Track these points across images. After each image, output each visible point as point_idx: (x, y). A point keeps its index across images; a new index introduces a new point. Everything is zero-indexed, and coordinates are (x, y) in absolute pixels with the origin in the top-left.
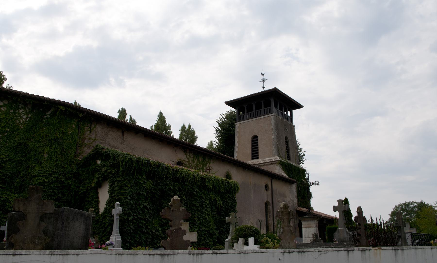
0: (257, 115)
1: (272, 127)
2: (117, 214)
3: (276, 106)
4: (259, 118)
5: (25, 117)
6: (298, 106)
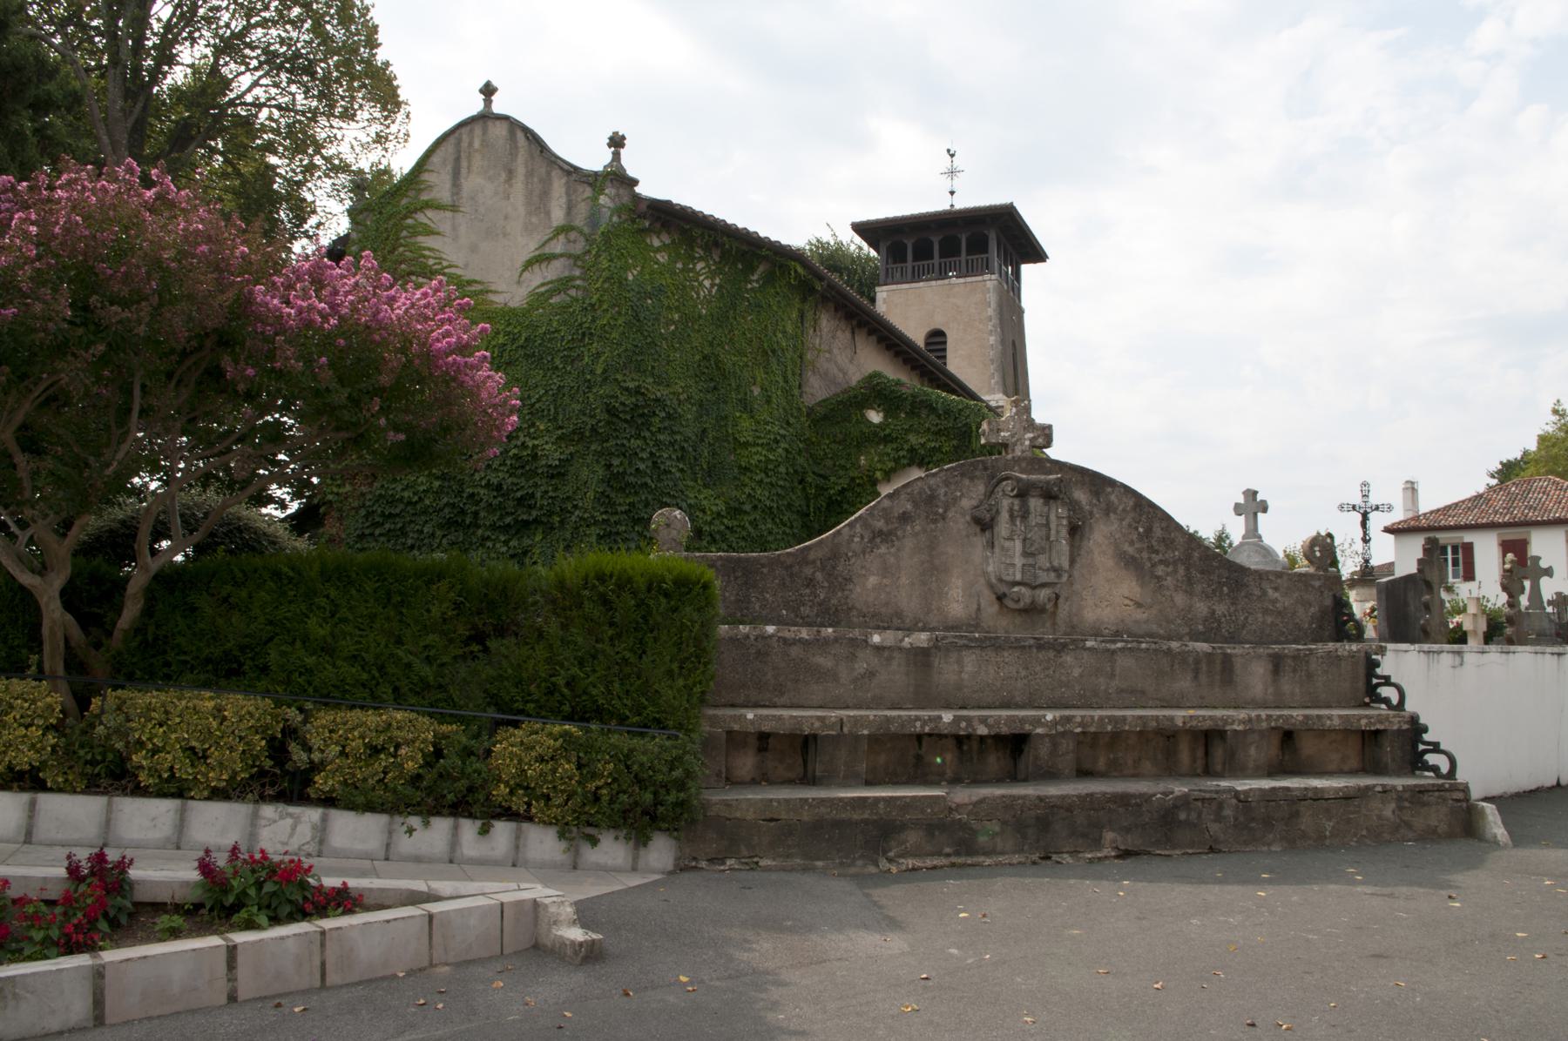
1: (990, 312)
5: (707, 283)
6: (1038, 255)
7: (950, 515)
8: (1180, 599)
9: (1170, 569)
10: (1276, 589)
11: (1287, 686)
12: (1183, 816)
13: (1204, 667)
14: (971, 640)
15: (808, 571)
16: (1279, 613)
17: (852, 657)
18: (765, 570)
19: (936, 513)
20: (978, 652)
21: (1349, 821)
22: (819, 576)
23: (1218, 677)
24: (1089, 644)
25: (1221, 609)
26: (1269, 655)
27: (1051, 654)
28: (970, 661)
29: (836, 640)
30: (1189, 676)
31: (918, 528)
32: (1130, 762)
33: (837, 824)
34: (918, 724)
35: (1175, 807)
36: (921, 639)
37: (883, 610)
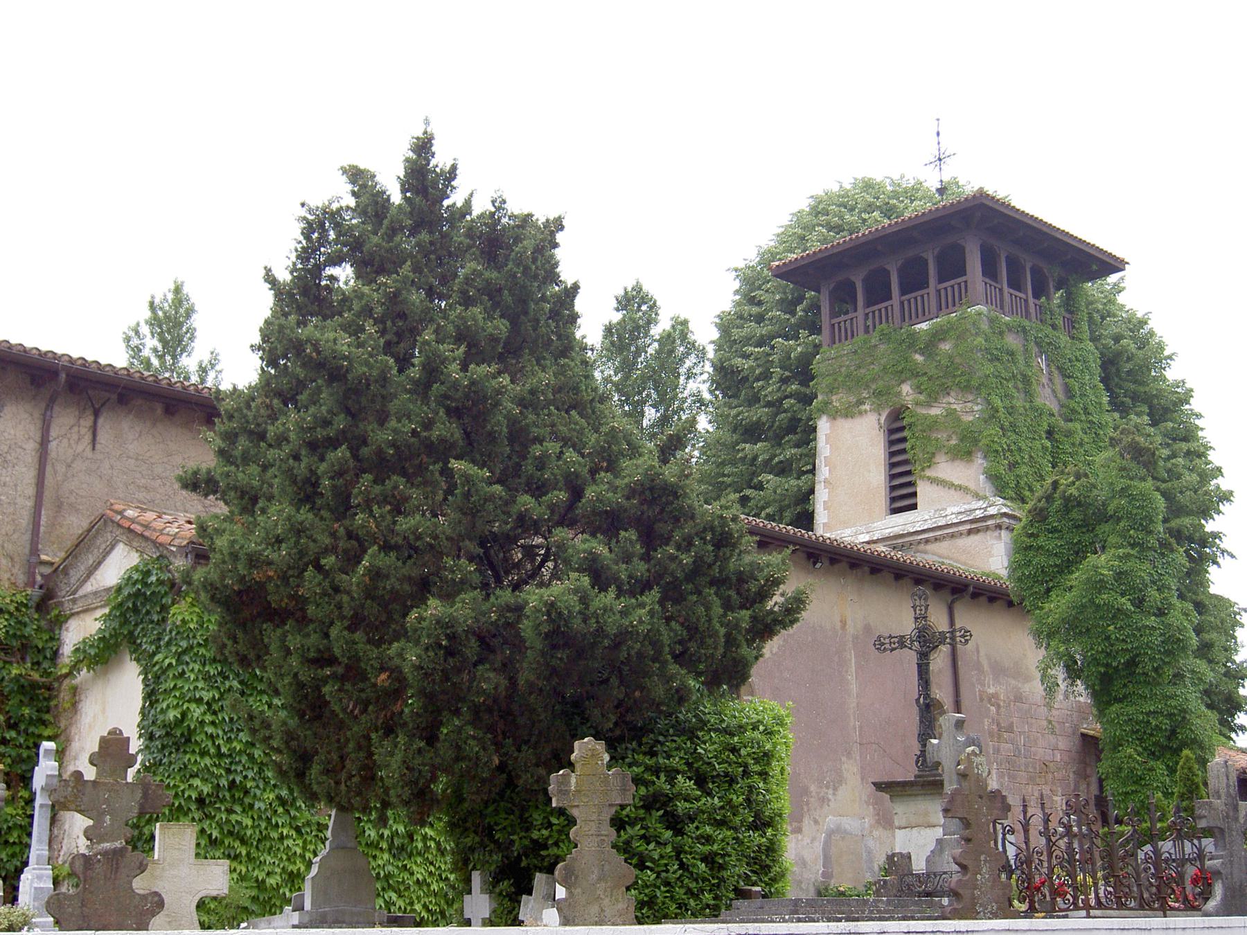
2: (42, 788)
3: (990, 271)
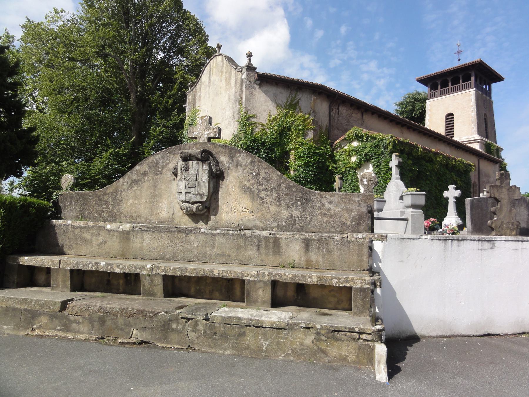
0: (454, 91)
4: (456, 94)
6: (499, 79)
7: (164, 171)
8: (273, 209)
9: (269, 193)
10: (330, 203)
11: (314, 256)
12: (174, 326)
13: (263, 244)
14: (148, 228)
15: (106, 198)
16: (332, 216)
17: (98, 235)
18: (90, 198)
19: (158, 171)
20: (150, 233)
21: (279, 343)
22: (110, 200)
23: (271, 250)
24: (203, 231)
25: (296, 213)
26: (303, 239)
27: (184, 235)
28: (147, 237)
29: (93, 227)
30: (255, 249)
31: (150, 178)
32: (207, 292)
33: (14, 309)
34: (90, 266)
35: (170, 320)
36: (127, 227)
37: (134, 214)
